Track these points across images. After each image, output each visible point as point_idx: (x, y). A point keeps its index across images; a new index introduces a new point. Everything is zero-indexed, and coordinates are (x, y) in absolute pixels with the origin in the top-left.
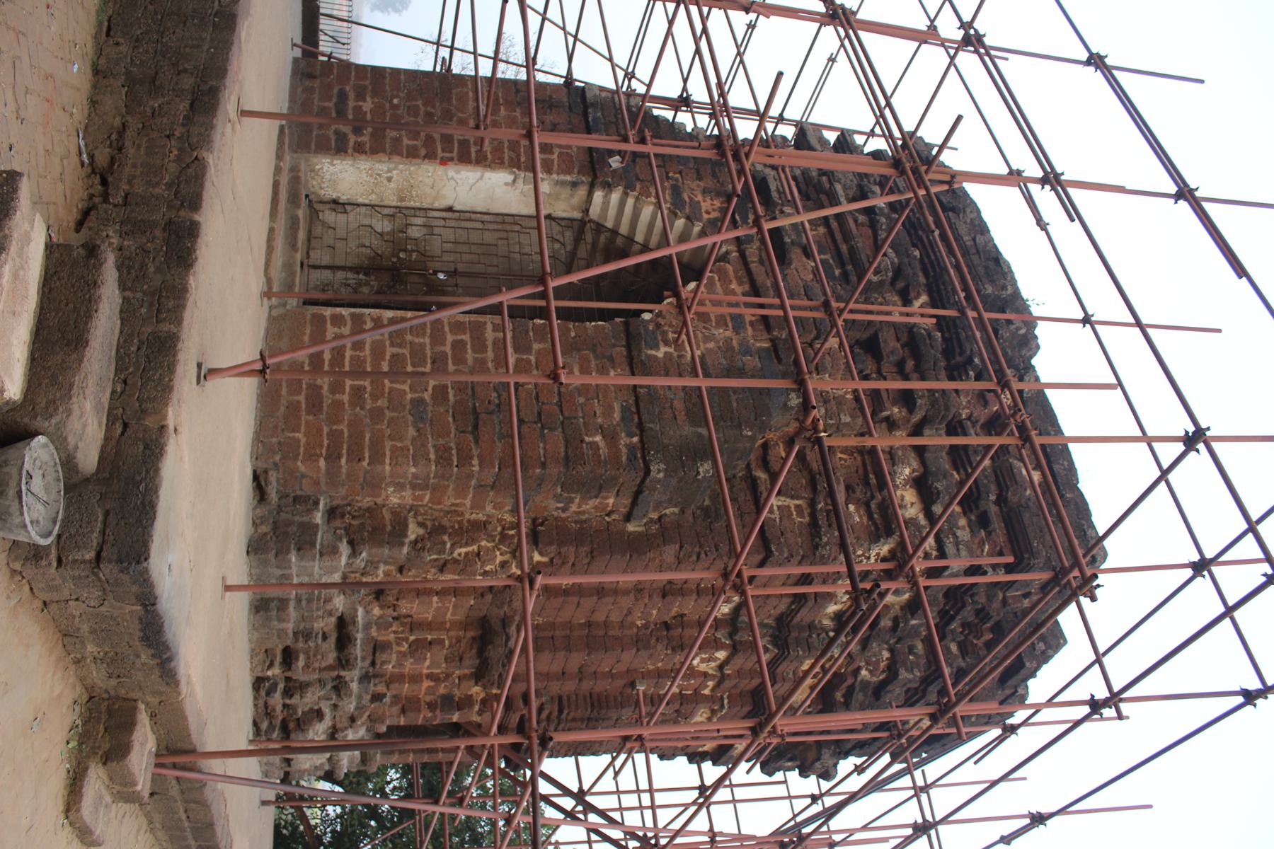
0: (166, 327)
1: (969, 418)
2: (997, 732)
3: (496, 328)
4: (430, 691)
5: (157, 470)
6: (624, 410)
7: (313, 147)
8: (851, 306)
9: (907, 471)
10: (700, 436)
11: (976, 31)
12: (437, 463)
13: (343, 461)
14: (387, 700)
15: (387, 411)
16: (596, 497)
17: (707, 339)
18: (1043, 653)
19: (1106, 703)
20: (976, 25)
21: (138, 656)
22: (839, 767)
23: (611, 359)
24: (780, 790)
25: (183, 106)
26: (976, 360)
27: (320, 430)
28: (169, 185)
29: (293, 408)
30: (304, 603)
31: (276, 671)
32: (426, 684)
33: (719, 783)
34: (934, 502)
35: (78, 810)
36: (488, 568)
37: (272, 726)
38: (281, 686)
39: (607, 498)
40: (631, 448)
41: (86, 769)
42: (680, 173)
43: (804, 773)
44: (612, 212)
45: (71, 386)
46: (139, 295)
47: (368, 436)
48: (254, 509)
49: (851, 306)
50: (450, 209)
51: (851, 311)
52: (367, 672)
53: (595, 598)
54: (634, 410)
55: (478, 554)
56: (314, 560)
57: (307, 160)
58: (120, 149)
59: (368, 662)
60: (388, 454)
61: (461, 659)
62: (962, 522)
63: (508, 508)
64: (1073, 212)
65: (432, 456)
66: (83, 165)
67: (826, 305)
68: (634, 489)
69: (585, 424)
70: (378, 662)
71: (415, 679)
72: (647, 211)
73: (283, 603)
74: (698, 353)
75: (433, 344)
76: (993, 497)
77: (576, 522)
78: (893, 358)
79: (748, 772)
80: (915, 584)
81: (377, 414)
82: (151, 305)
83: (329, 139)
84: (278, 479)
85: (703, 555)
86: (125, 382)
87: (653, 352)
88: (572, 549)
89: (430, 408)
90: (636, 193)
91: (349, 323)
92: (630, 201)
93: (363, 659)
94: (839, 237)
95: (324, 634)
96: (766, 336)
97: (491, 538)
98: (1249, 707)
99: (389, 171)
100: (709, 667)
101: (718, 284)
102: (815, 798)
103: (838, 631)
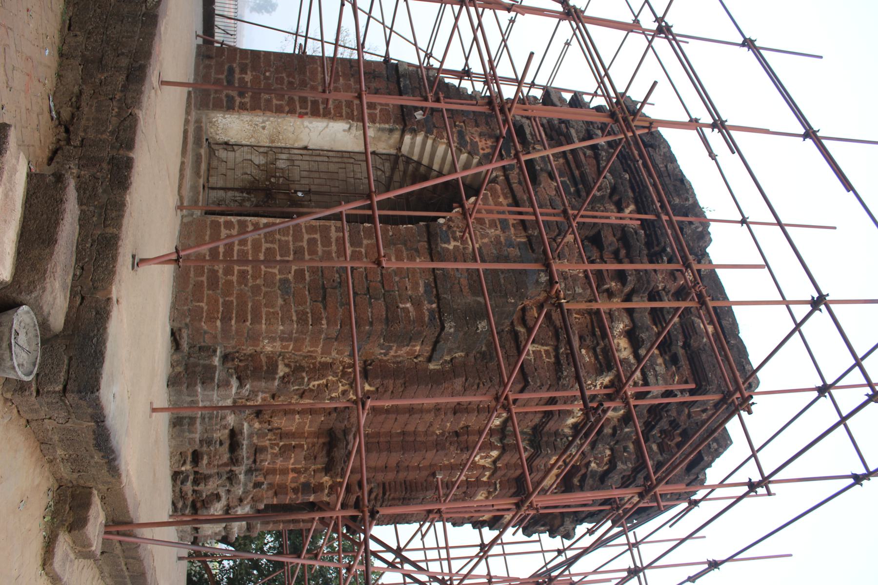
0: (110, 230)
1: (664, 289)
2: (684, 505)
3: (338, 230)
4: (294, 480)
5: (105, 329)
6: (427, 285)
7: (211, 106)
8: (582, 212)
9: (621, 326)
10: (479, 303)
11: (666, 23)
12: (298, 322)
13: (233, 322)
14: (264, 486)
15: (263, 288)
16: (408, 345)
17: (483, 236)
18: (716, 450)
19: (759, 484)
20: (666, 19)
21: (92, 457)
22: (576, 530)
23: (417, 250)
24: (536, 547)
25: (121, 78)
26: (668, 249)
27: (217, 301)
28: (112, 133)
29: (198, 286)
30: (207, 420)
31: (187, 467)
32: (292, 475)
33: (493, 542)
34: (640, 347)
35: (51, 564)
36: (333, 395)
37: (185, 506)
38: (191, 477)
39: (415, 346)
40: (431, 311)
41: (57, 536)
42: (464, 122)
43: (552, 535)
44: (417, 150)
45: (45, 271)
46: (92, 208)
47: (250, 305)
48: (172, 355)
49: (582, 212)
50: (305, 148)
51: (582, 216)
52: (251, 468)
53: (407, 415)
54: (433, 285)
55: (327, 386)
56: (213, 390)
57: (207, 115)
58: (78, 108)
59: (251, 460)
60: (264, 316)
61: (315, 458)
62: (660, 361)
63: (347, 353)
64: (734, 148)
65: (294, 318)
66: (52, 119)
67: (565, 212)
68: (434, 340)
69: (400, 295)
70: (258, 460)
71: (284, 472)
72: (441, 148)
73: (192, 420)
74: (477, 246)
75: (294, 241)
76: (680, 344)
77: (394, 363)
78: (611, 248)
79: (514, 534)
80: (627, 403)
81: (256, 289)
82: (100, 215)
83: (221, 100)
84: (188, 335)
85: (481, 385)
86: (82, 268)
87: (446, 246)
88: (391, 382)
89: (292, 285)
90: (433, 136)
91: (237, 227)
92: (430, 142)
93: (248, 458)
94: (573, 166)
95: (221, 441)
96: (524, 234)
97: (335, 374)
98: (858, 486)
99: (263, 122)
100: (487, 462)
101: (490, 198)
102: (560, 552)
103: (575, 437)
